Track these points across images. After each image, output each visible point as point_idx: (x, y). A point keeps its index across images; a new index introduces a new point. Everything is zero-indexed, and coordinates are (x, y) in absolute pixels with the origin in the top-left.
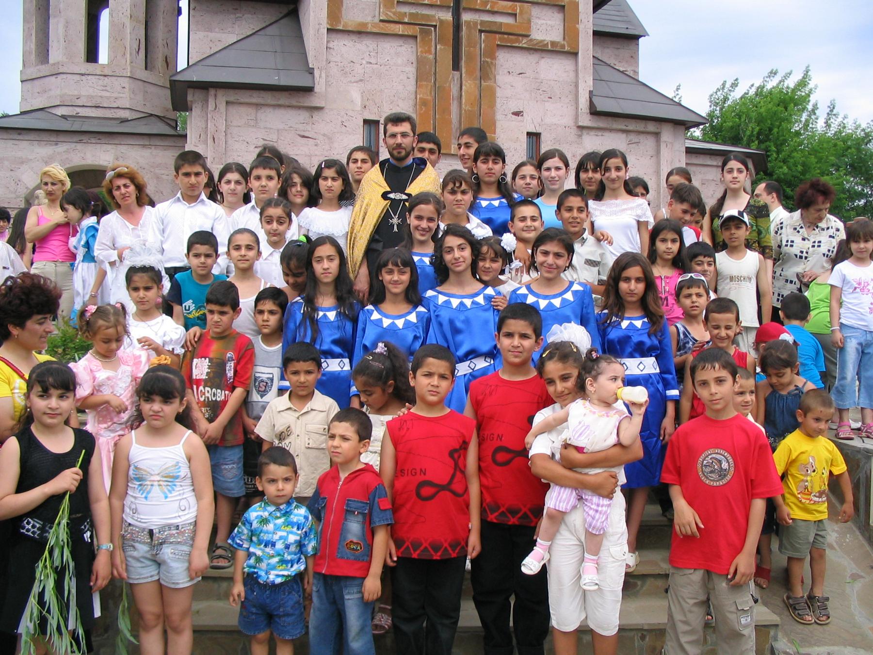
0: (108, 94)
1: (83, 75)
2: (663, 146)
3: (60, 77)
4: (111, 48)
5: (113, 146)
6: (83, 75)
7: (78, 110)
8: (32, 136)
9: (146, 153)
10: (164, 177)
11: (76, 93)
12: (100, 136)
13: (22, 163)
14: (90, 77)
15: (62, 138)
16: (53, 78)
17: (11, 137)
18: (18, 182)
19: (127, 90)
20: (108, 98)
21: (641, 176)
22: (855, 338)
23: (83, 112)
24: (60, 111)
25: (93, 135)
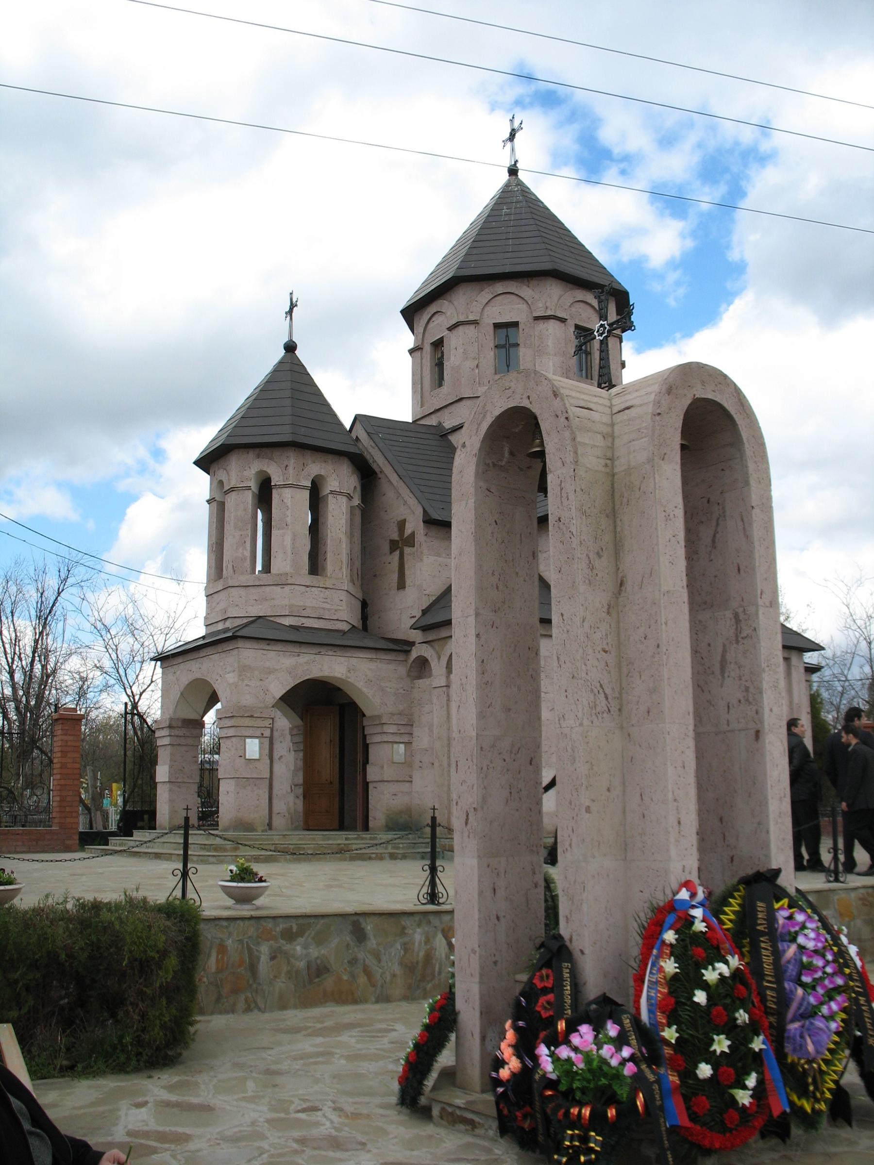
0: (328, 606)
1: (307, 586)
2: (793, 668)
3: (287, 588)
4: (755, 783)
5: (347, 659)
6: (307, 586)
7: (304, 620)
8: (279, 647)
9: (373, 665)
10: (389, 690)
11: (302, 604)
12: (335, 649)
13: (270, 673)
14: (313, 589)
15: (304, 649)
16: (278, 589)
17: (261, 647)
18: (266, 691)
19: (344, 603)
20: (329, 610)
21: (538, 414)
22: (204, 752)
23: (309, 623)
24: (287, 622)
25: (330, 648)
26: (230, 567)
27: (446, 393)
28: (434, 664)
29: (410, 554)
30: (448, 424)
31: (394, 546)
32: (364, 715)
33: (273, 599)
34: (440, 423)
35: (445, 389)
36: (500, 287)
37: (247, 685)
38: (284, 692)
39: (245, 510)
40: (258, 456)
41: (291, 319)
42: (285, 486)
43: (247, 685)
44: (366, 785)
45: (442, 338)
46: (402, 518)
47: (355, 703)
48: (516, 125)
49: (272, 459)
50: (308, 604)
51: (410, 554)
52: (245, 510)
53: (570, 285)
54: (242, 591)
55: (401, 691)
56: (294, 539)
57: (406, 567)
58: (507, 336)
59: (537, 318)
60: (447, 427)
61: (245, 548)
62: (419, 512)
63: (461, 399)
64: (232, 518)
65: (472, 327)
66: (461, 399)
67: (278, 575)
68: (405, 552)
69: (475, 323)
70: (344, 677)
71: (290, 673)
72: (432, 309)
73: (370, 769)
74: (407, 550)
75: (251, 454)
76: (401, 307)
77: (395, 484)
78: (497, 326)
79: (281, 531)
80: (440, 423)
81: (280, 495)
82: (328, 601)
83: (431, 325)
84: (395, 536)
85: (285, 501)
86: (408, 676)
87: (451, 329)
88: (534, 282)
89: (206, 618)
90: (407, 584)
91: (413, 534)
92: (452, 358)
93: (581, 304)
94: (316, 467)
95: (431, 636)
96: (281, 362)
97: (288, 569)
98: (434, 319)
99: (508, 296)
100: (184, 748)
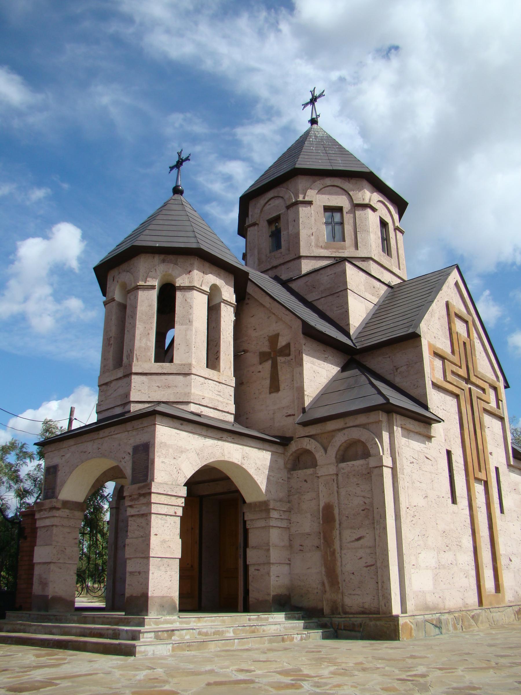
0: (221, 399)
1: (206, 378)
6: (206, 378)
7: (203, 408)
8: (191, 427)
11: (201, 393)
13: (182, 452)
16: (181, 378)
18: (179, 471)
20: (222, 403)
28: (319, 455)
29: (284, 362)
31: (264, 357)
32: (244, 502)
37: (163, 462)
38: (193, 472)
40: (163, 261)
43: (163, 462)
44: (246, 567)
46: (276, 332)
47: (237, 491)
48: (175, 171)
49: (176, 264)
50: (206, 395)
51: (284, 362)
55: (280, 480)
60: (284, 279)
67: (182, 365)
68: (279, 361)
70: (239, 463)
71: (198, 454)
72: (271, 194)
73: (250, 553)
74: (280, 359)
75: (157, 259)
76: (94, 266)
77: (268, 305)
78: (327, 209)
79: (184, 327)
82: (221, 394)
83: (267, 207)
84: (266, 349)
86: (286, 467)
88: (353, 181)
89: (98, 405)
90: (281, 387)
91: (288, 345)
92: (291, 228)
95: (312, 430)
98: (270, 203)
99: (335, 188)
100: (67, 530)
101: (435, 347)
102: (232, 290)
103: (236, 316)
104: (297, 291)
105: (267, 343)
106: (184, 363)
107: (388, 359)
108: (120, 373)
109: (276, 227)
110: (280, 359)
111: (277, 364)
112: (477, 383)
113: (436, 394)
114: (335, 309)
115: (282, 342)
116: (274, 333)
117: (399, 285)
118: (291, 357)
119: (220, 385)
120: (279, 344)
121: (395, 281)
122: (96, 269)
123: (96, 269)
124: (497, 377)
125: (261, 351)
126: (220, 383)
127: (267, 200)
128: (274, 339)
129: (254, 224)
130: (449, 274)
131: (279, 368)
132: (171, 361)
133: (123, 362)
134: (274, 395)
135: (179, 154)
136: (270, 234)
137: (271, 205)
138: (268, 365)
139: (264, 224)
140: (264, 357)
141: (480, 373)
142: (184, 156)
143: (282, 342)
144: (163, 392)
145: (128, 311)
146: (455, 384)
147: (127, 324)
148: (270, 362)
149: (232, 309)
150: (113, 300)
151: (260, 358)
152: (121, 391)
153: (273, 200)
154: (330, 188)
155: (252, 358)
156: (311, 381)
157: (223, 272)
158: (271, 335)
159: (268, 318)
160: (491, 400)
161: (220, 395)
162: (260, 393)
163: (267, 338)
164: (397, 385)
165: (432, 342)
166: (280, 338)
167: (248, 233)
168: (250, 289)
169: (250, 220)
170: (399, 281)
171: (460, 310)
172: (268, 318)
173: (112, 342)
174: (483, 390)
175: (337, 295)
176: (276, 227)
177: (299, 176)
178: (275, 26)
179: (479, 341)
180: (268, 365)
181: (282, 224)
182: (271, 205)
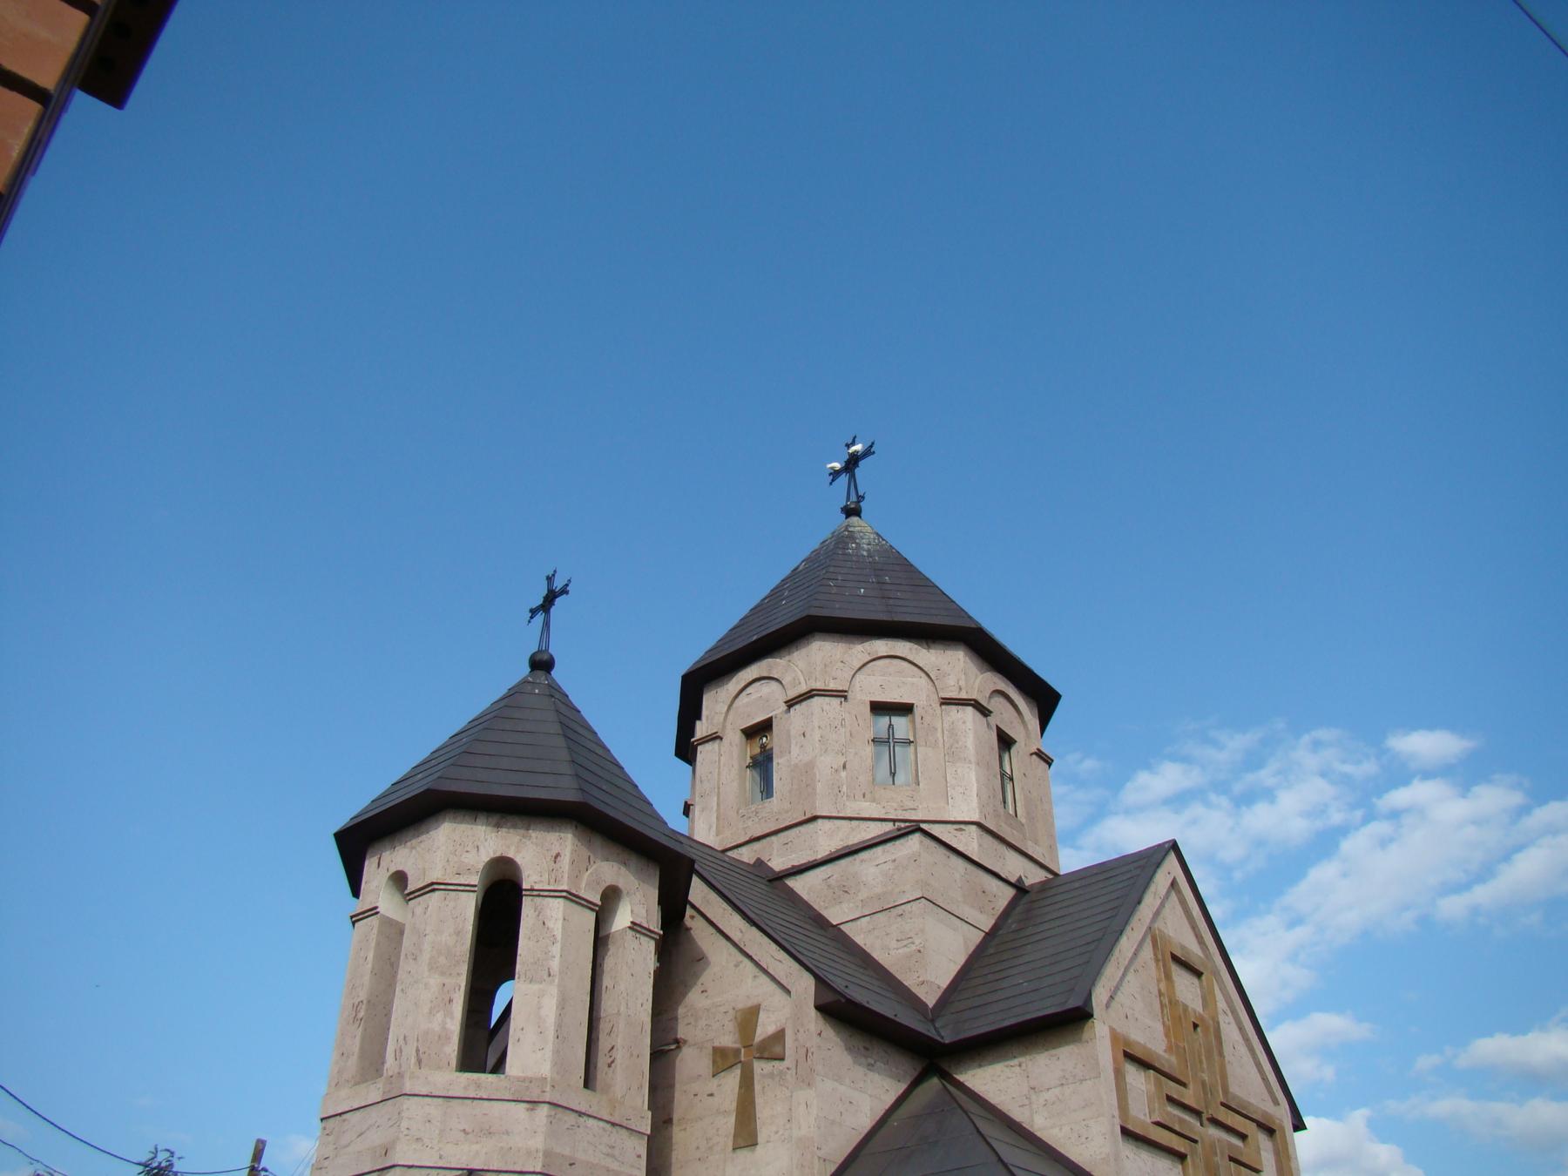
1: (581, 1114)
6: (581, 1114)
11: (567, 1152)
14: (591, 1122)
26: (410, 1051)
27: (780, 808)
29: (771, 1075)
30: (778, 864)
31: (723, 1059)
33: (507, 1133)
34: (760, 863)
35: (775, 803)
36: (881, 646)
39: (458, 933)
41: (547, 624)
42: (554, 894)
45: (770, 720)
46: (754, 1001)
48: (540, 617)
51: (771, 1075)
52: (458, 933)
53: (598, 841)
54: (434, 1108)
56: (562, 1005)
57: (759, 1101)
58: (891, 725)
59: (947, 702)
60: (777, 869)
61: (449, 1014)
62: (804, 985)
63: (814, 818)
64: (427, 947)
65: (835, 701)
66: (814, 818)
67: (524, 1080)
69: (841, 695)
74: (760, 1068)
76: (336, 829)
78: (879, 708)
79: (536, 987)
80: (760, 863)
81: (539, 912)
82: (616, 1152)
83: (743, 699)
84: (728, 1040)
85: (550, 924)
87: (790, 704)
90: (762, 1137)
91: (779, 1036)
92: (795, 750)
93: (1001, 700)
94: (610, 870)
96: (514, 693)
97: (546, 1069)
98: (749, 690)
101: (1127, 1042)
102: (654, 894)
103: (659, 960)
104: (805, 897)
105: (731, 1026)
106: (529, 1074)
107: (1017, 1069)
108: (373, 1092)
109: (763, 746)
110: (760, 1068)
111: (752, 1078)
112: (1229, 1122)
113: (1131, 1156)
114: (894, 944)
115: (766, 1027)
116: (750, 1004)
117: (1044, 886)
118: (786, 1063)
119: (615, 1130)
120: (759, 1030)
121: (1034, 876)
122: (336, 835)
123: (336, 835)
124: (1276, 1103)
125: (717, 1044)
126: (614, 1124)
127: (742, 684)
128: (748, 1019)
129: (715, 737)
130: (1159, 865)
131: (757, 1087)
132: (499, 1067)
133: (387, 1066)
134: (744, 1154)
135: (550, 579)
136: (749, 760)
137: (753, 697)
138: (732, 1080)
139: (733, 738)
140: (723, 1059)
141: (1235, 1097)
142: (558, 584)
143: (766, 1027)
144: (475, 1147)
145: (407, 941)
146: (1177, 1128)
147: (401, 975)
148: (737, 1071)
149: (652, 944)
150: (373, 911)
151: (714, 1062)
152: (376, 1138)
153: (757, 684)
154: (887, 661)
155: (691, 1064)
156: (833, 1122)
157: (634, 860)
158: (740, 1006)
159: (736, 966)
160: (1264, 1162)
161: (613, 1156)
162: (710, 1148)
163: (731, 1014)
164: (1038, 1134)
165: (1121, 1028)
166: (762, 1015)
167: (699, 757)
168: (692, 921)
169: (701, 729)
170: (1041, 875)
171: (1183, 947)
172: (736, 966)
173: (361, 1014)
174: (1243, 1137)
175: (899, 910)
176: (763, 746)
177: (818, 635)
178: (688, 929)
179: (1230, 1018)
180: (732, 1080)
181: (775, 740)
182: (753, 697)
